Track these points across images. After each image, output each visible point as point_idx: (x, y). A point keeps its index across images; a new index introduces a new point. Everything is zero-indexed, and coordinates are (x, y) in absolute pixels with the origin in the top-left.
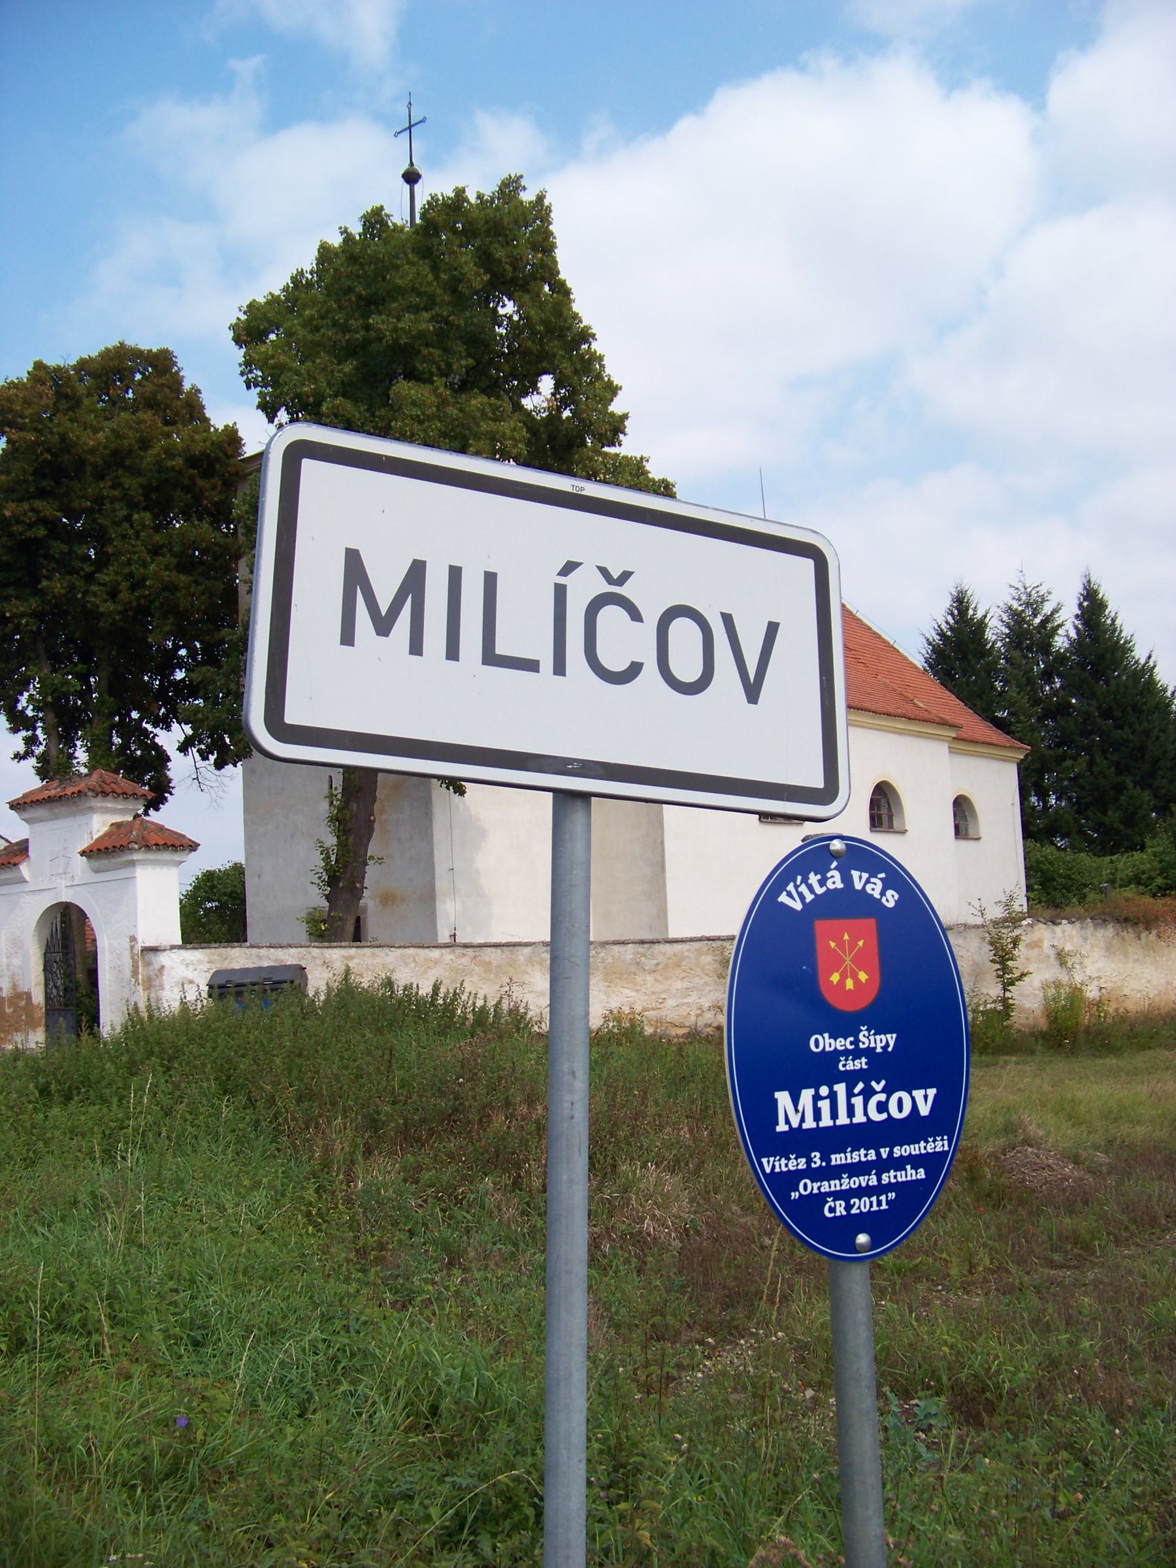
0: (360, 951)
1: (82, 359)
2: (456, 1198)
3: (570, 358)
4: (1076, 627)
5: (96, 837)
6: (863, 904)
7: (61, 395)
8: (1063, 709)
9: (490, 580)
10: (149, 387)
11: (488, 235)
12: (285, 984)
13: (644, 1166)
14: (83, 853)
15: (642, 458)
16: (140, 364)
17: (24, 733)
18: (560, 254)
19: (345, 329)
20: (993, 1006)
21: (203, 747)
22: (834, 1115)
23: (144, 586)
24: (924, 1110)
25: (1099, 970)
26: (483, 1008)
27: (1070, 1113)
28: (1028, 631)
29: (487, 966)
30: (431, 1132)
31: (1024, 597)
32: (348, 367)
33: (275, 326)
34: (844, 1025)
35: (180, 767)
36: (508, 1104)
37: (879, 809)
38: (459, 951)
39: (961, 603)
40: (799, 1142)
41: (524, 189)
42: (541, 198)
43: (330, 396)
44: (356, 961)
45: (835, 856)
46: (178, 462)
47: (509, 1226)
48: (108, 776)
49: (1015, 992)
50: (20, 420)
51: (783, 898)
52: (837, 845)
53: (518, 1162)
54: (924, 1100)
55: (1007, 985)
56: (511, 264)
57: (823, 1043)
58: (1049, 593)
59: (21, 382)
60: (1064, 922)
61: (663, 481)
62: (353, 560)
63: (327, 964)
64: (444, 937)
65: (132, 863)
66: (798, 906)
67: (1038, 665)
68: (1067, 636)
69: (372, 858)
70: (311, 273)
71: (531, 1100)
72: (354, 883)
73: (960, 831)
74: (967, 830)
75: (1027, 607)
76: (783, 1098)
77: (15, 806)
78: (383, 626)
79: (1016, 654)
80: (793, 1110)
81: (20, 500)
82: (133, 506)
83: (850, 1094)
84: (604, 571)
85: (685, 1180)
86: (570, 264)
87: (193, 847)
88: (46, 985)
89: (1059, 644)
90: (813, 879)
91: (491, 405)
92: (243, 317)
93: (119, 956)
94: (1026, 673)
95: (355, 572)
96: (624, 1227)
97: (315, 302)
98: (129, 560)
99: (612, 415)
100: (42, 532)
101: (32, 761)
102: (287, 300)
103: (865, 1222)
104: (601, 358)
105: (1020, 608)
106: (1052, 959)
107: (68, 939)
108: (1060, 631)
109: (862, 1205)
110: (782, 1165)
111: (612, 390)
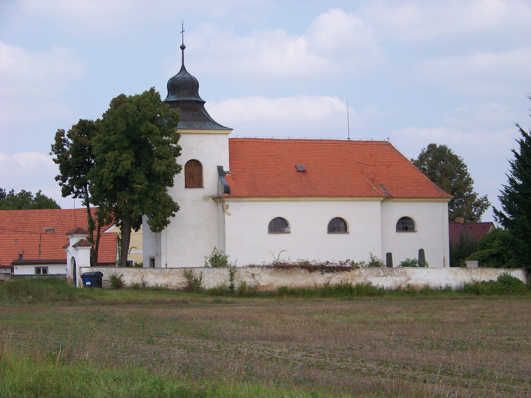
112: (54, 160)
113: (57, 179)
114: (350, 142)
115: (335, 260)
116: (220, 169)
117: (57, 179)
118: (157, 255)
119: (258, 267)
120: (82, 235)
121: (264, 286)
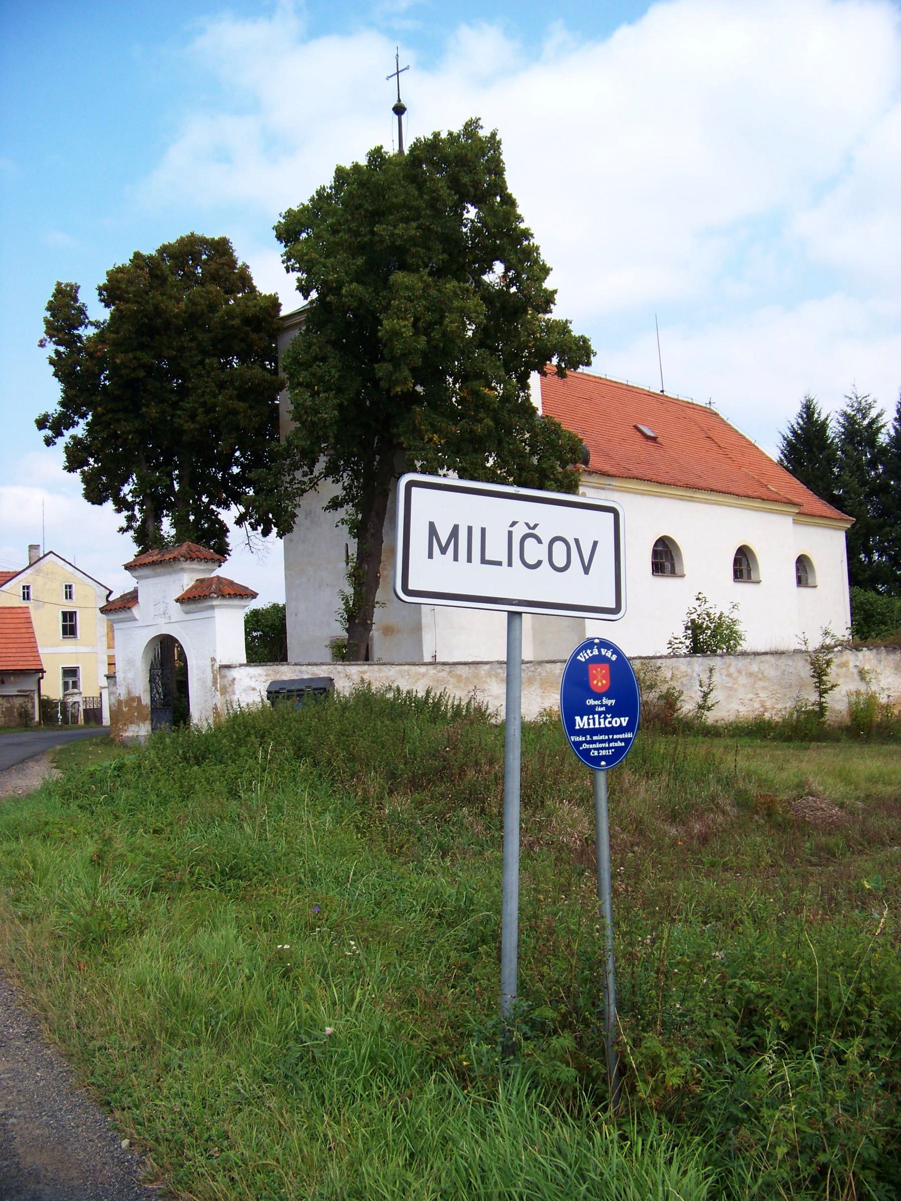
0: (370, 667)
1: (164, 245)
2: (445, 820)
3: (516, 252)
4: (895, 428)
5: (186, 589)
6: (605, 659)
7: (153, 275)
8: (884, 489)
9: (483, 530)
10: (213, 266)
11: (457, 166)
12: (322, 689)
13: (561, 802)
14: (177, 600)
15: (567, 321)
16: (206, 249)
17: (126, 513)
18: (507, 176)
19: (357, 234)
20: (811, 708)
21: (253, 521)
22: (594, 724)
23: (215, 411)
24: (624, 724)
25: (889, 683)
26: (459, 706)
27: (845, 777)
28: (858, 430)
29: (459, 677)
30: (429, 781)
31: (856, 405)
32: (360, 261)
33: (305, 227)
34: (598, 697)
35: (236, 536)
36: (477, 764)
37: (741, 566)
38: (440, 667)
39: (808, 409)
40: (582, 732)
41: (482, 127)
42: (494, 135)
43: (347, 282)
44: (368, 674)
45: (596, 644)
46: (236, 322)
47: (478, 836)
48: (194, 546)
49: (827, 697)
50: (126, 296)
51: (579, 657)
52: (597, 641)
53: (483, 799)
54: (624, 721)
55: (822, 693)
56: (473, 187)
57: (591, 702)
58: (875, 402)
59: (124, 267)
60: (865, 649)
61: (582, 337)
62: (432, 526)
63: (348, 677)
64: (427, 658)
65: (212, 607)
66: (583, 660)
67: (866, 455)
68: (888, 434)
69: (377, 603)
70: (331, 188)
71: (491, 762)
72: (366, 620)
73: (802, 581)
74: (807, 580)
75: (858, 412)
76: (578, 718)
77: (128, 567)
78: (443, 551)
79: (849, 448)
80: (581, 722)
81: (126, 352)
82: (205, 353)
83: (599, 718)
84: (527, 524)
85: (587, 812)
86: (514, 184)
87: (254, 595)
88: (151, 691)
89: (881, 440)
90: (589, 651)
91: (460, 288)
92: (283, 221)
93: (203, 672)
94: (856, 462)
95: (433, 530)
96: (548, 838)
97: (335, 213)
98: (203, 392)
99: (545, 291)
100: (142, 374)
101: (131, 533)
102: (314, 207)
103: (604, 758)
104: (537, 248)
105: (853, 413)
106: (857, 678)
107: (168, 660)
108: (883, 430)
109: (603, 753)
110: (577, 739)
111: (546, 271)
114: (660, 399)
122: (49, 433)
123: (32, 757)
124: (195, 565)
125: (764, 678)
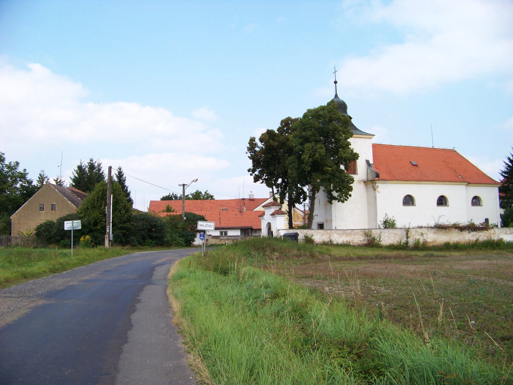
100: (268, 160)
112: (249, 157)
113: (249, 171)
114: (433, 149)
115: (478, 221)
116: (368, 162)
117: (249, 171)
118: (327, 221)
119: (425, 227)
120: (276, 207)
121: (430, 242)
122: (251, 173)
123: (344, 246)
124: (275, 207)
125: (397, 235)
